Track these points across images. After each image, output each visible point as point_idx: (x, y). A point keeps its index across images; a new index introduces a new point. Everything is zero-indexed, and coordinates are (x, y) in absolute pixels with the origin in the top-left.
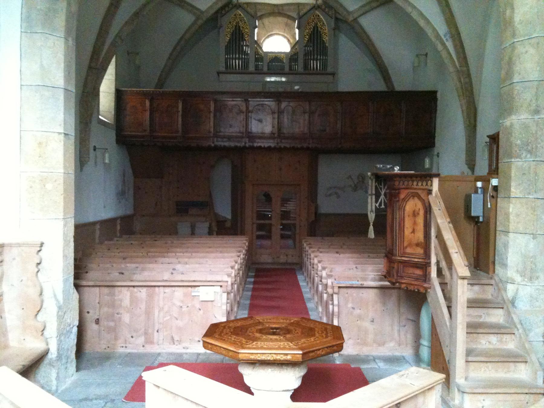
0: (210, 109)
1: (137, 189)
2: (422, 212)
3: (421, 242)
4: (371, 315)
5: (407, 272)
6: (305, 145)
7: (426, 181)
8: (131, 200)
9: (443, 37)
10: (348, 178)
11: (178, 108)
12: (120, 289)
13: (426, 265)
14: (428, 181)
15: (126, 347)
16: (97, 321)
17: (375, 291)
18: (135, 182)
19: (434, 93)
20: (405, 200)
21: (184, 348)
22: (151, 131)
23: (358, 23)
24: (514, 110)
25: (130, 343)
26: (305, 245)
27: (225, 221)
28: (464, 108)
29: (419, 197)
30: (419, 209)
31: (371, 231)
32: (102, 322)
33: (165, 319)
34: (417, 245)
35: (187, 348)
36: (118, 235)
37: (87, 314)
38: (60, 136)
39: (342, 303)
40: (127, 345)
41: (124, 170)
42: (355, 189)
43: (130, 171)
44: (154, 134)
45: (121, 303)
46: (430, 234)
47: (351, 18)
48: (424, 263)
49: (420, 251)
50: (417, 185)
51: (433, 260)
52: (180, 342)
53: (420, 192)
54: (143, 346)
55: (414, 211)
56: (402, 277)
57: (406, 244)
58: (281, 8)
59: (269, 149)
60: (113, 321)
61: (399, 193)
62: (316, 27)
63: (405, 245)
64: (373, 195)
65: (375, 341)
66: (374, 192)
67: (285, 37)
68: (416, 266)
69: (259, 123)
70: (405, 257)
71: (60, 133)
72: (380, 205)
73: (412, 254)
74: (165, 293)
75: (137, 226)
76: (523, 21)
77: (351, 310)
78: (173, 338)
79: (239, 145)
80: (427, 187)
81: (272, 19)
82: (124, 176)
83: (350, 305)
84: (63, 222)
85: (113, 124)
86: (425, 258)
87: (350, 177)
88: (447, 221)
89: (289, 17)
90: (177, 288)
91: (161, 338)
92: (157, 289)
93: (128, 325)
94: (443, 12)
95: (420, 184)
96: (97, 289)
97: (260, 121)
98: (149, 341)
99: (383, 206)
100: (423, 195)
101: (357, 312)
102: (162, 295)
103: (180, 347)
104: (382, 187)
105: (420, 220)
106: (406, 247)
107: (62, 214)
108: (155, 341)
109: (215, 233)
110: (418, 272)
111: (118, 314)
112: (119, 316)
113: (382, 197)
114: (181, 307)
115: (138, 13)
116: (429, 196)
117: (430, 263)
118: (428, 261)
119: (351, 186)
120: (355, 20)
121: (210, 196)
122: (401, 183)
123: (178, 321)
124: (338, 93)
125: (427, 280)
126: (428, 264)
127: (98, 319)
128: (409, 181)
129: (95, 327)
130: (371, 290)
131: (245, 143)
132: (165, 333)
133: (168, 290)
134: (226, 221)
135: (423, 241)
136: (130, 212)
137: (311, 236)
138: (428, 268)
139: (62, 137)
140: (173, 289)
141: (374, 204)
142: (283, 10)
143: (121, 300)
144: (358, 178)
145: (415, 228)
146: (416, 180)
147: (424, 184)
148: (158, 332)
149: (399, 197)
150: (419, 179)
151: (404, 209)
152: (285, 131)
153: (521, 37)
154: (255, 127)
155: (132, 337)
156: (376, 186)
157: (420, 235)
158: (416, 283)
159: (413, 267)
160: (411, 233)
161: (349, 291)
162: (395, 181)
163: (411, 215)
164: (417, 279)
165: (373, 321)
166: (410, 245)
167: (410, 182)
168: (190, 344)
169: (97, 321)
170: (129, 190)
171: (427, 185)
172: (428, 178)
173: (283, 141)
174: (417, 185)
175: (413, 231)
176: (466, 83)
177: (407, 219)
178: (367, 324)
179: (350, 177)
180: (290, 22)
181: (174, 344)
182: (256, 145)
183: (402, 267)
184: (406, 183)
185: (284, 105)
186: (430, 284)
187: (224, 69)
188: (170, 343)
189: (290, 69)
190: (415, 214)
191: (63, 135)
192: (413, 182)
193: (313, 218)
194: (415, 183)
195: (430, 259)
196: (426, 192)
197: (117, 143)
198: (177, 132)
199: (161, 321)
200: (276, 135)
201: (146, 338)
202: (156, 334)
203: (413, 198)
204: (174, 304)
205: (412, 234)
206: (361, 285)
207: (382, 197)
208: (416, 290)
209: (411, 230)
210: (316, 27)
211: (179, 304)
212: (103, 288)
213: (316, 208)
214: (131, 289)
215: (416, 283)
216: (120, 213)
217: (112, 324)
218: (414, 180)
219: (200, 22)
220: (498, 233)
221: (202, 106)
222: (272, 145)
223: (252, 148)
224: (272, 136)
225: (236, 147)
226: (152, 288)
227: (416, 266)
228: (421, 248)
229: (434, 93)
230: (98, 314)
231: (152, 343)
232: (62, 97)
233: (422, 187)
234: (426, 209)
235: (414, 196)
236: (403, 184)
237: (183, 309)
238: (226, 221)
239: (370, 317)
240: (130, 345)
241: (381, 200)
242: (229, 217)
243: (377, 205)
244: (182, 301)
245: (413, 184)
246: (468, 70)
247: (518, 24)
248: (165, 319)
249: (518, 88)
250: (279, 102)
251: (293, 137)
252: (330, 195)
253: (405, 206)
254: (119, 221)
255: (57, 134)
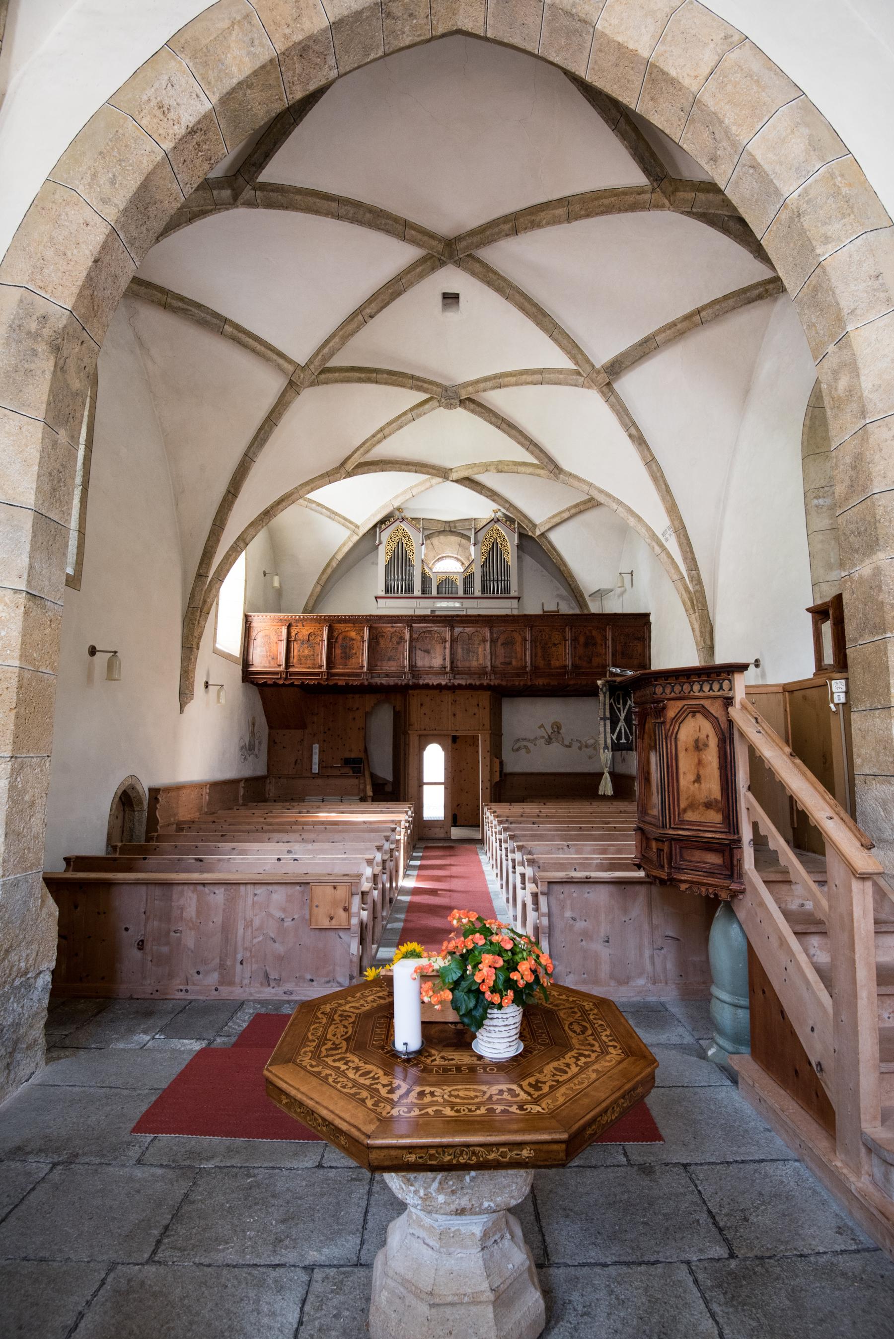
0: (362, 637)
1: (272, 742)
2: (713, 742)
3: (716, 800)
4: (604, 929)
5: (688, 858)
6: (485, 682)
7: (718, 681)
8: (264, 757)
9: (660, 537)
10: (540, 727)
11: (322, 636)
12: (180, 888)
13: (729, 845)
14: (724, 680)
15: (187, 991)
16: (141, 945)
17: (611, 888)
18: (270, 734)
19: (647, 615)
20: (679, 719)
21: (285, 993)
22: (288, 665)
23: (546, 538)
24: (881, 542)
25: (194, 984)
26: (488, 814)
27: (385, 783)
28: (697, 626)
29: (707, 714)
30: (707, 736)
31: (606, 783)
32: (148, 946)
33: (255, 941)
34: (708, 805)
35: (291, 994)
36: (241, 801)
37: (124, 933)
38: (17, 596)
39: (555, 910)
40: (188, 988)
41: (254, 718)
42: (549, 741)
43: (264, 719)
44: (291, 670)
45: (182, 913)
46: (734, 782)
47: (538, 533)
48: (727, 842)
49: (715, 817)
50: (701, 690)
51: (747, 834)
52: (278, 981)
53: (706, 703)
54: (216, 989)
55: (697, 741)
56: (680, 869)
57: (683, 805)
58: (452, 525)
59: (439, 687)
60: (168, 943)
61: (664, 708)
62: (494, 544)
63: (682, 806)
64: (608, 718)
65: (612, 977)
66: (608, 715)
67: (458, 559)
68: (709, 846)
69: (426, 654)
70: (683, 829)
71: (16, 591)
72: (619, 737)
73: (700, 824)
74: (255, 895)
75: (271, 789)
76: (880, 387)
77: (571, 922)
78: (267, 976)
79: (400, 682)
80: (721, 692)
81: (442, 538)
82: (254, 724)
83: (568, 914)
84: (10, 763)
85: (238, 656)
86: (726, 830)
87: (542, 726)
88: (784, 753)
89: (463, 536)
90: (275, 887)
91: (247, 975)
92: (242, 888)
93: (192, 951)
94: (663, 499)
95: (706, 688)
96: (143, 889)
97: (428, 652)
98: (227, 979)
99: (623, 741)
100: (715, 709)
101: (580, 925)
102: (250, 900)
103: (280, 990)
104: (621, 706)
105: (711, 756)
106: (685, 811)
107: (10, 747)
108: (237, 980)
109: (370, 799)
110: (714, 859)
111: (175, 932)
112: (178, 934)
113: (622, 724)
114: (283, 920)
115: (268, 512)
116: (730, 709)
117: (739, 841)
118: (736, 837)
119: (543, 737)
120: (543, 535)
121: (366, 750)
122: (668, 691)
123: (277, 945)
124: (525, 615)
125: (735, 876)
126: (737, 843)
127: (142, 941)
128: (684, 683)
129: (137, 954)
130: (602, 887)
131: (407, 679)
132: (255, 967)
133: (260, 890)
134: (386, 784)
135: (719, 798)
136: (261, 771)
137: (495, 802)
138: (735, 851)
139: (22, 599)
140: (270, 888)
141: (609, 735)
142: (455, 527)
143: (182, 909)
144: (552, 728)
145: (701, 773)
146: (698, 682)
147: (716, 686)
148: (241, 963)
149: (665, 716)
150: (704, 678)
151: (676, 738)
152: (459, 664)
153: (879, 413)
154: (422, 661)
155: (198, 973)
156: (611, 705)
157: (712, 787)
158: (710, 880)
159: (698, 848)
160: (694, 782)
161: (567, 889)
162: (656, 685)
163: (691, 748)
164: (711, 874)
165: (608, 941)
166: (692, 806)
167: (686, 687)
168: (297, 985)
169: (141, 945)
170: (260, 743)
171: (721, 688)
172: (724, 675)
173: (457, 676)
174: (701, 690)
175: (698, 779)
176: (697, 591)
177: (682, 755)
178: (597, 946)
179: (542, 726)
180: (464, 541)
181: (269, 985)
182: (421, 682)
183: (678, 850)
184: (677, 688)
185: (458, 630)
186: (742, 884)
187: (383, 594)
188: (262, 984)
189: (465, 592)
190: (699, 746)
191: (24, 594)
192: (692, 686)
193: (497, 778)
194: (696, 687)
195: (738, 833)
196: (719, 702)
197: (243, 681)
198: (321, 666)
199: (248, 944)
200: (448, 669)
201: (222, 975)
202: (238, 967)
203: (693, 716)
204: (269, 915)
205: (696, 785)
206: (587, 878)
207: (622, 724)
208: (712, 896)
209: (692, 778)
210: (494, 544)
211: (279, 914)
212: (151, 888)
213: (501, 763)
214: (200, 888)
215: (710, 880)
216: (247, 773)
217: (165, 949)
218: (694, 682)
219: (356, 538)
220: (858, 780)
221: (353, 634)
222: (443, 683)
223: (416, 687)
224: (442, 671)
225: (396, 686)
226: (234, 887)
227: (709, 846)
228: (718, 811)
229: (647, 615)
230: (143, 932)
231: (231, 983)
232: (28, 526)
233: (711, 693)
234: (723, 734)
235: (694, 713)
236: (673, 691)
237: (286, 924)
238: (386, 784)
239: (602, 934)
240: (193, 987)
241: (620, 730)
242: (390, 778)
243: (614, 737)
244: (284, 910)
245: (692, 690)
246: (699, 575)
247: (870, 392)
248: (255, 941)
249: (882, 502)
250: (452, 628)
251: (470, 673)
252: (518, 750)
253: (677, 733)
254: (242, 784)
255: (12, 592)
